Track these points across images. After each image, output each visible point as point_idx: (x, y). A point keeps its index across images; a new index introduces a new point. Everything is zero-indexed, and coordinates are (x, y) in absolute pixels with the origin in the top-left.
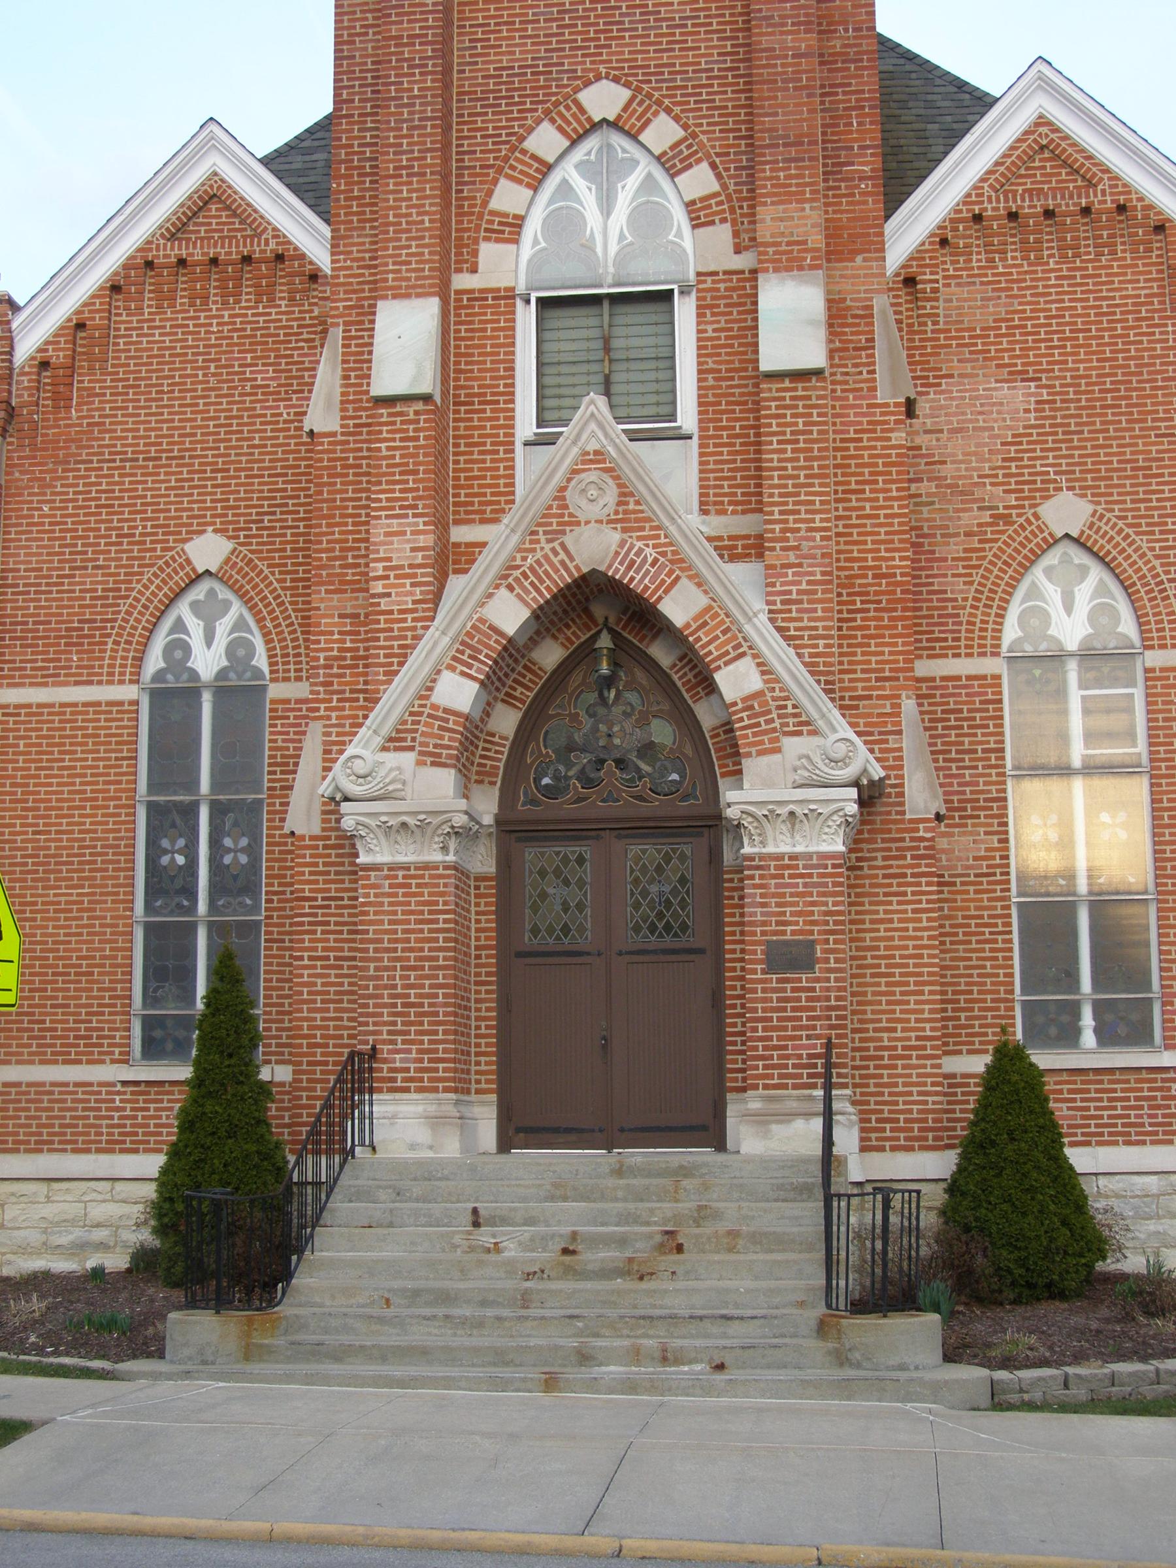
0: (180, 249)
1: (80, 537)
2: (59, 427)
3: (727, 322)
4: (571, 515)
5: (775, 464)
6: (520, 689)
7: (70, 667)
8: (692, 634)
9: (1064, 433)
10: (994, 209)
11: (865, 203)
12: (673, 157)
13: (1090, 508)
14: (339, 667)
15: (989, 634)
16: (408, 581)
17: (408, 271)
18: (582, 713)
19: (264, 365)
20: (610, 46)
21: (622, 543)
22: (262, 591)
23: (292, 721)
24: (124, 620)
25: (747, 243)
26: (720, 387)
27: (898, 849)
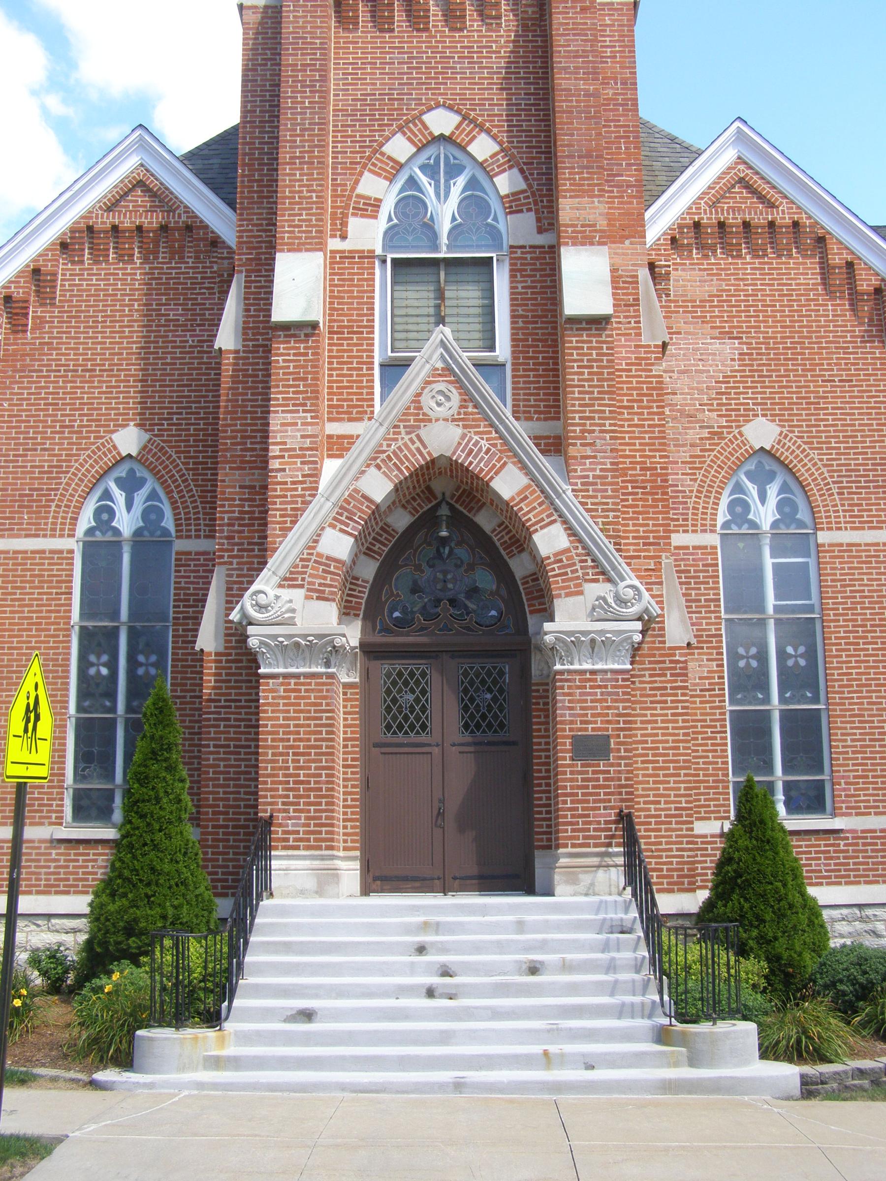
0: (114, 218)
1: (32, 427)
2: (17, 344)
3: (532, 282)
4: (424, 414)
5: (576, 383)
6: (378, 545)
7: (22, 524)
8: (516, 505)
9: (759, 376)
10: (708, 219)
11: (631, 203)
12: (493, 164)
13: (779, 430)
14: (240, 525)
15: (708, 517)
16: (299, 460)
17: (299, 232)
18: (424, 565)
19: (175, 305)
20: (446, 84)
21: (463, 436)
22: (171, 471)
23: (192, 568)
24: (64, 489)
25: (546, 226)
26: (528, 328)
27: (660, 669)
